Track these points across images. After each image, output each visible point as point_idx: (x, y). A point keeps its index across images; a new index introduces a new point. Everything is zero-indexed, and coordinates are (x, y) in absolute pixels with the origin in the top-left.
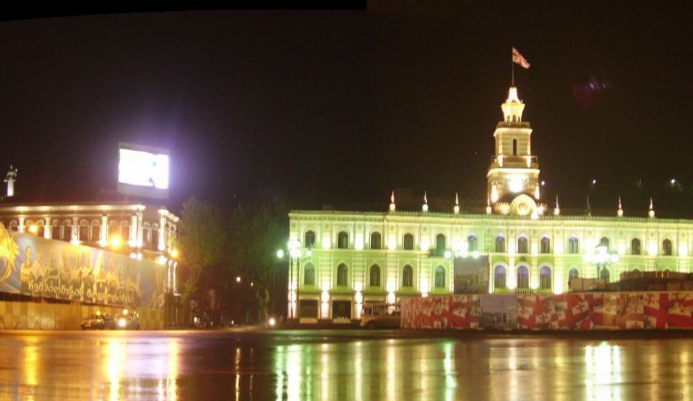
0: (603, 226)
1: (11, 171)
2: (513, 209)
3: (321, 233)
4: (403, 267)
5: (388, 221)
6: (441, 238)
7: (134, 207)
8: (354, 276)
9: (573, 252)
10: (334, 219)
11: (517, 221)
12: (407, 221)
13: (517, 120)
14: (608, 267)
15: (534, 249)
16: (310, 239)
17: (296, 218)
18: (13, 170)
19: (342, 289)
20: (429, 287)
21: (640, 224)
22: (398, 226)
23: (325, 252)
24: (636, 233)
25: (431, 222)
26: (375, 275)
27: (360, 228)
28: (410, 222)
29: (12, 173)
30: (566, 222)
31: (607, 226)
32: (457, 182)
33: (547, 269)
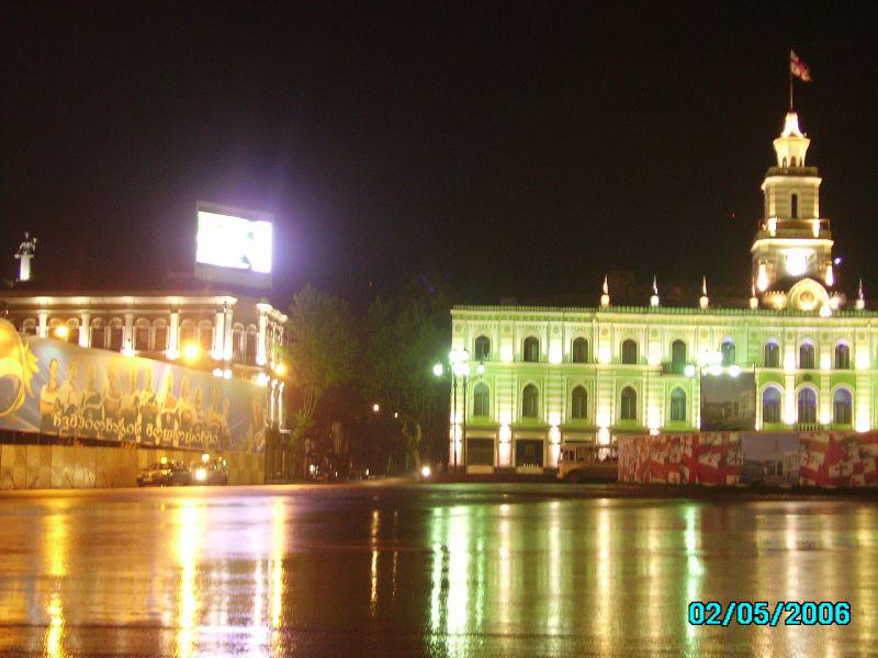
3: (499, 339)
4: (621, 389)
5: (598, 321)
6: (679, 347)
12: (626, 322)
15: (826, 362)
16: (482, 348)
17: (461, 317)
18: (30, 240)
19: (529, 422)
22: (613, 329)
23: (553, 369)
25: (664, 322)
27: (556, 332)
32: (702, 259)
33: (845, 393)
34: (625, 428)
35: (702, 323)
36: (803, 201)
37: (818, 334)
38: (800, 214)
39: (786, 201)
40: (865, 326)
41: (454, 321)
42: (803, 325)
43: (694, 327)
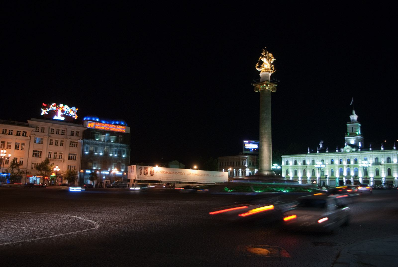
0: (376, 154)
1: (321, 141)
2: (344, 150)
3: (298, 160)
4: (312, 170)
5: (307, 157)
6: (313, 161)
7: (246, 156)
8: (370, 172)
9: (313, 164)
10: (293, 157)
11: (346, 154)
12: (312, 156)
13: (356, 121)
14: (367, 168)
15: (352, 162)
16: (287, 163)
17: (283, 157)
18: (322, 141)
19: (377, 177)
20: (385, 176)
21: (390, 152)
22: (292, 158)
23: (299, 166)
24: (389, 155)
25: (319, 156)
26: (304, 172)
27: (300, 159)
28: (313, 156)
29: (321, 142)
30: (362, 153)
31: (377, 154)
32: (335, 144)
33: (357, 169)
34: (388, 178)
35: (394, 153)
36: (351, 129)
37: (343, 157)
38: (353, 131)
39: (351, 129)
40: (360, 154)
41: (282, 158)
42: (347, 155)
43: (392, 154)
